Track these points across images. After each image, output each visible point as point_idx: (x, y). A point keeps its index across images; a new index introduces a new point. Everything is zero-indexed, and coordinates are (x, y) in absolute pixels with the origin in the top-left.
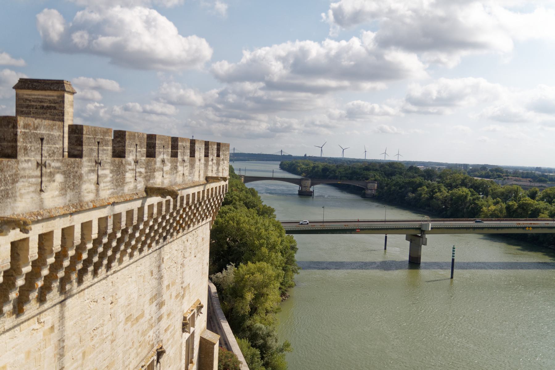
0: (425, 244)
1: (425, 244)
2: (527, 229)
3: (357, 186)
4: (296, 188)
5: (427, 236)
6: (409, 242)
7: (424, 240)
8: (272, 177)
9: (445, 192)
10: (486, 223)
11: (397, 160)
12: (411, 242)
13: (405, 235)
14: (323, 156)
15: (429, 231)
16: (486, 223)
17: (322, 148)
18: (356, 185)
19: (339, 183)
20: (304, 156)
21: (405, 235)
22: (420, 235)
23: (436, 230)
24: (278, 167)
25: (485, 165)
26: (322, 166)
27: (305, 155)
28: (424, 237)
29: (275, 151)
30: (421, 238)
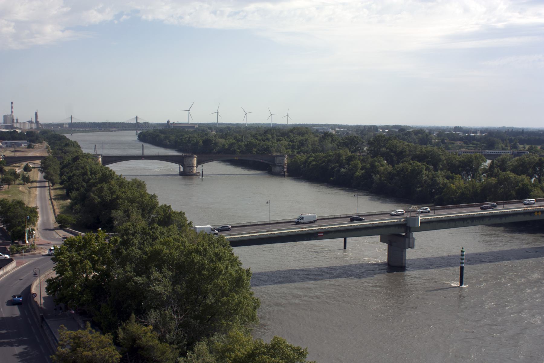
0: (412, 247)
1: (412, 247)
2: (536, 214)
3: (260, 162)
4: (176, 168)
5: (415, 235)
6: (385, 246)
7: (411, 240)
8: (142, 155)
9: (384, 166)
10: (500, 209)
11: (286, 123)
12: (390, 245)
13: (379, 237)
14: (191, 122)
15: (418, 227)
16: (500, 209)
17: (189, 111)
18: (259, 160)
19: (237, 160)
20: (166, 122)
21: (379, 237)
22: (404, 234)
23: (429, 225)
24: (136, 138)
25: (396, 125)
26: (38, 128)
27: (168, 122)
28: (411, 237)
29: (127, 117)
30: (407, 238)
